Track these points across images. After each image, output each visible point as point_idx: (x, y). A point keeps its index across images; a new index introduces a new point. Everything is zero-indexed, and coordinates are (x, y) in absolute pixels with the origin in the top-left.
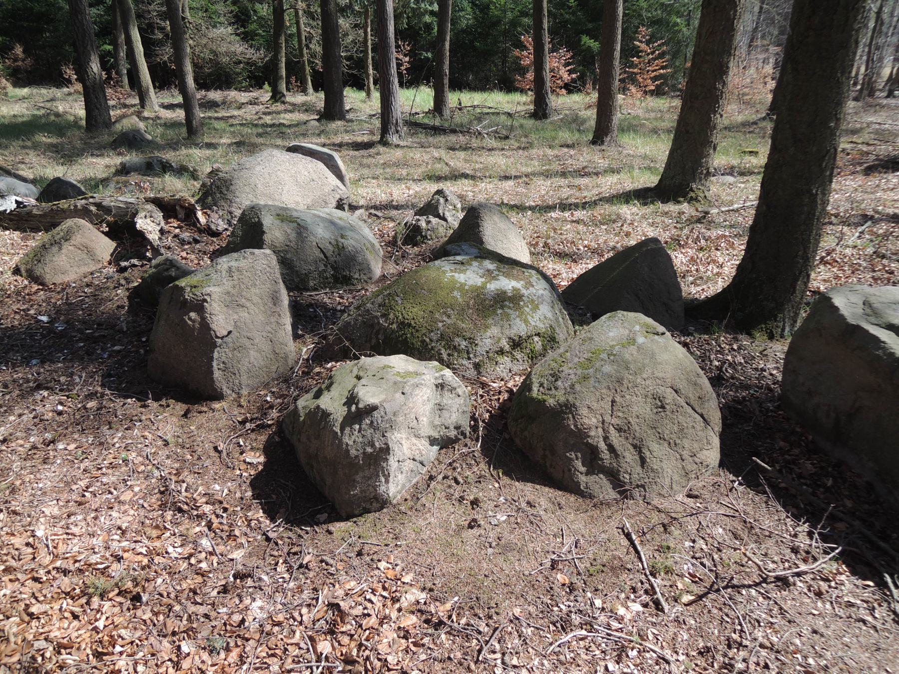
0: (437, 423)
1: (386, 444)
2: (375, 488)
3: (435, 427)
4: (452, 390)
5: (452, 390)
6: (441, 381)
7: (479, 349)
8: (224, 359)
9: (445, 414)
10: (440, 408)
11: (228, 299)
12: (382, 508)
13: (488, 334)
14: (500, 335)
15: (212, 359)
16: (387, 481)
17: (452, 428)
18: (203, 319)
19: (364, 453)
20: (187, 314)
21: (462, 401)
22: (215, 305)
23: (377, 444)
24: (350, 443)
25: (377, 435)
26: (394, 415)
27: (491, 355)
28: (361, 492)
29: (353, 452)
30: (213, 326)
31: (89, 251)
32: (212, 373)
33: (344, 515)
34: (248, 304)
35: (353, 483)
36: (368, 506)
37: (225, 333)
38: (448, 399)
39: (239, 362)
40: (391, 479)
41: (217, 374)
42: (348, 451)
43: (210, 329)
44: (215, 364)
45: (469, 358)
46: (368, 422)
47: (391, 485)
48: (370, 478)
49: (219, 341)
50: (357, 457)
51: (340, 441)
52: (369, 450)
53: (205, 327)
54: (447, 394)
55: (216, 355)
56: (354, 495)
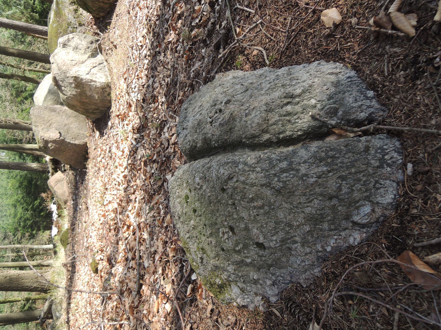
0: (83, 52)
1: (72, 77)
2: (96, 88)
3: (85, 53)
4: (69, 40)
5: (69, 40)
6: (62, 45)
7: (72, 22)
8: (71, 138)
9: (80, 46)
10: (76, 48)
11: (45, 130)
12: (110, 87)
13: (67, 14)
14: (68, 9)
15: (69, 143)
16: (95, 82)
17: (90, 45)
18: (51, 142)
19: (75, 88)
20: (49, 148)
21: (77, 37)
22: (46, 136)
23: (71, 81)
24: (70, 93)
25: (67, 80)
26: (60, 70)
27: (76, 16)
28: (97, 93)
29: (74, 93)
30: (55, 138)
31: (58, 181)
32: (75, 144)
33: (109, 104)
34: (50, 122)
35: (91, 97)
36: (107, 93)
37: (59, 134)
38: (73, 44)
39: (74, 132)
40: (94, 79)
41: (77, 142)
42: (73, 95)
43: (55, 140)
44: (72, 142)
45: (76, 28)
46: (61, 83)
47: (97, 80)
48: (91, 89)
49: (61, 138)
50: (76, 92)
51: (69, 97)
52: (73, 85)
53: (54, 141)
54: (70, 43)
55: (68, 141)
56: (99, 97)
